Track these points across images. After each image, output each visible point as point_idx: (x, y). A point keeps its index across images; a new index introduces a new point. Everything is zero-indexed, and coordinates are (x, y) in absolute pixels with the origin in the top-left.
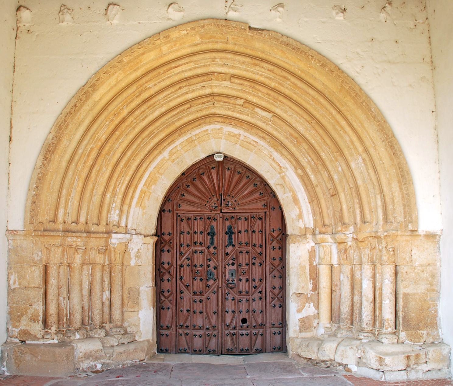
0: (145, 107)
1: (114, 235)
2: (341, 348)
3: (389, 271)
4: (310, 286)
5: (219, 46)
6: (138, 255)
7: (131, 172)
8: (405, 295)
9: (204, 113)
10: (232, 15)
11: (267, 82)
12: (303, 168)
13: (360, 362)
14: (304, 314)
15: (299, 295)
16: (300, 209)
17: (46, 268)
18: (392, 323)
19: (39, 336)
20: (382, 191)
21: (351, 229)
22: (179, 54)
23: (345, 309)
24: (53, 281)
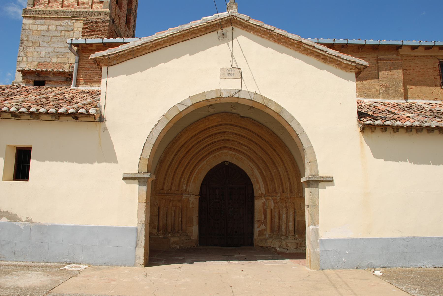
0: (198, 145)
1: (184, 195)
2: (273, 241)
3: (291, 212)
4: (263, 217)
5: (228, 122)
6: (193, 203)
7: (191, 169)
8: (298, 221)
9: (221, 146)
10: (233, 111)
11: (247, 136)
12: (260, 169)
13: (280, 247)
14: (260, 229)
15: (258, 221)
16: (259, 185)
17: (159, 208)
18: (293, 231)
19: (156, 234)
20: (289, 181)
21: (279, 194)
22: (212, 125)
23: (276, 227)
24: (161, 213)
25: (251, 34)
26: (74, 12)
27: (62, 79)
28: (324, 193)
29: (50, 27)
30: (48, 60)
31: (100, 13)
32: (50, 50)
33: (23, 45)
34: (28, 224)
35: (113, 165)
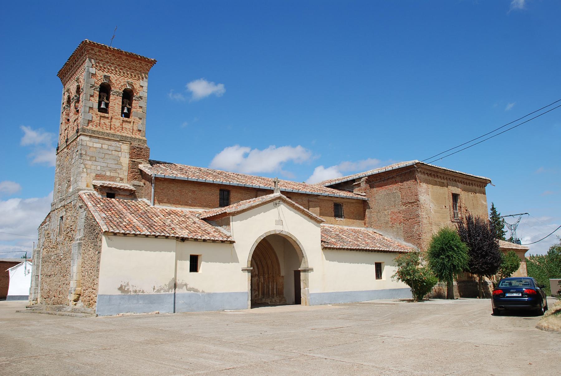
3: (275, 283)
25: (285, 204)
26: (121, 136)
27: (128, 194)
28: (310, 274)
29: (103, 146)
30: (103, 173)
31: (140, 140)
32: (104, 165)
33: (83, 158)
34: (203, 293)
35: (237, 264)
